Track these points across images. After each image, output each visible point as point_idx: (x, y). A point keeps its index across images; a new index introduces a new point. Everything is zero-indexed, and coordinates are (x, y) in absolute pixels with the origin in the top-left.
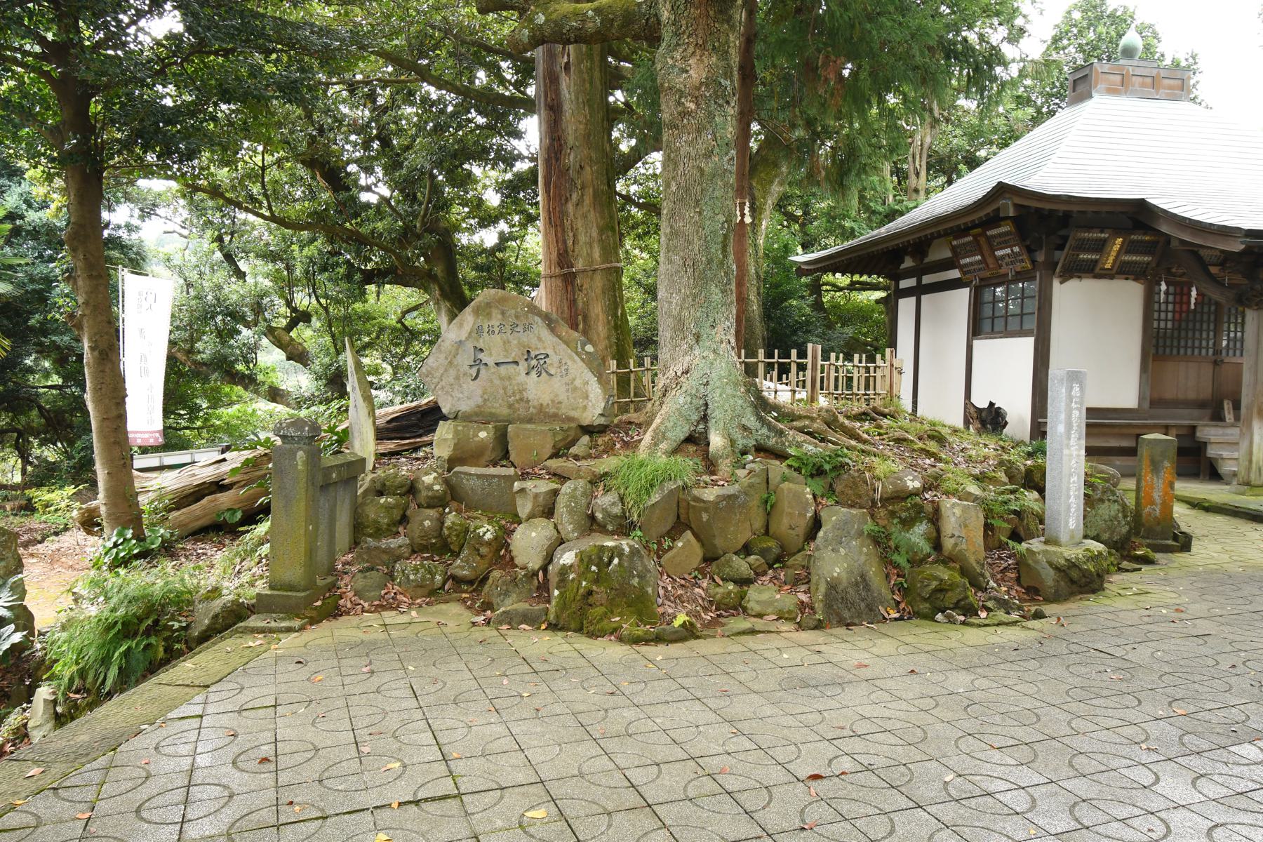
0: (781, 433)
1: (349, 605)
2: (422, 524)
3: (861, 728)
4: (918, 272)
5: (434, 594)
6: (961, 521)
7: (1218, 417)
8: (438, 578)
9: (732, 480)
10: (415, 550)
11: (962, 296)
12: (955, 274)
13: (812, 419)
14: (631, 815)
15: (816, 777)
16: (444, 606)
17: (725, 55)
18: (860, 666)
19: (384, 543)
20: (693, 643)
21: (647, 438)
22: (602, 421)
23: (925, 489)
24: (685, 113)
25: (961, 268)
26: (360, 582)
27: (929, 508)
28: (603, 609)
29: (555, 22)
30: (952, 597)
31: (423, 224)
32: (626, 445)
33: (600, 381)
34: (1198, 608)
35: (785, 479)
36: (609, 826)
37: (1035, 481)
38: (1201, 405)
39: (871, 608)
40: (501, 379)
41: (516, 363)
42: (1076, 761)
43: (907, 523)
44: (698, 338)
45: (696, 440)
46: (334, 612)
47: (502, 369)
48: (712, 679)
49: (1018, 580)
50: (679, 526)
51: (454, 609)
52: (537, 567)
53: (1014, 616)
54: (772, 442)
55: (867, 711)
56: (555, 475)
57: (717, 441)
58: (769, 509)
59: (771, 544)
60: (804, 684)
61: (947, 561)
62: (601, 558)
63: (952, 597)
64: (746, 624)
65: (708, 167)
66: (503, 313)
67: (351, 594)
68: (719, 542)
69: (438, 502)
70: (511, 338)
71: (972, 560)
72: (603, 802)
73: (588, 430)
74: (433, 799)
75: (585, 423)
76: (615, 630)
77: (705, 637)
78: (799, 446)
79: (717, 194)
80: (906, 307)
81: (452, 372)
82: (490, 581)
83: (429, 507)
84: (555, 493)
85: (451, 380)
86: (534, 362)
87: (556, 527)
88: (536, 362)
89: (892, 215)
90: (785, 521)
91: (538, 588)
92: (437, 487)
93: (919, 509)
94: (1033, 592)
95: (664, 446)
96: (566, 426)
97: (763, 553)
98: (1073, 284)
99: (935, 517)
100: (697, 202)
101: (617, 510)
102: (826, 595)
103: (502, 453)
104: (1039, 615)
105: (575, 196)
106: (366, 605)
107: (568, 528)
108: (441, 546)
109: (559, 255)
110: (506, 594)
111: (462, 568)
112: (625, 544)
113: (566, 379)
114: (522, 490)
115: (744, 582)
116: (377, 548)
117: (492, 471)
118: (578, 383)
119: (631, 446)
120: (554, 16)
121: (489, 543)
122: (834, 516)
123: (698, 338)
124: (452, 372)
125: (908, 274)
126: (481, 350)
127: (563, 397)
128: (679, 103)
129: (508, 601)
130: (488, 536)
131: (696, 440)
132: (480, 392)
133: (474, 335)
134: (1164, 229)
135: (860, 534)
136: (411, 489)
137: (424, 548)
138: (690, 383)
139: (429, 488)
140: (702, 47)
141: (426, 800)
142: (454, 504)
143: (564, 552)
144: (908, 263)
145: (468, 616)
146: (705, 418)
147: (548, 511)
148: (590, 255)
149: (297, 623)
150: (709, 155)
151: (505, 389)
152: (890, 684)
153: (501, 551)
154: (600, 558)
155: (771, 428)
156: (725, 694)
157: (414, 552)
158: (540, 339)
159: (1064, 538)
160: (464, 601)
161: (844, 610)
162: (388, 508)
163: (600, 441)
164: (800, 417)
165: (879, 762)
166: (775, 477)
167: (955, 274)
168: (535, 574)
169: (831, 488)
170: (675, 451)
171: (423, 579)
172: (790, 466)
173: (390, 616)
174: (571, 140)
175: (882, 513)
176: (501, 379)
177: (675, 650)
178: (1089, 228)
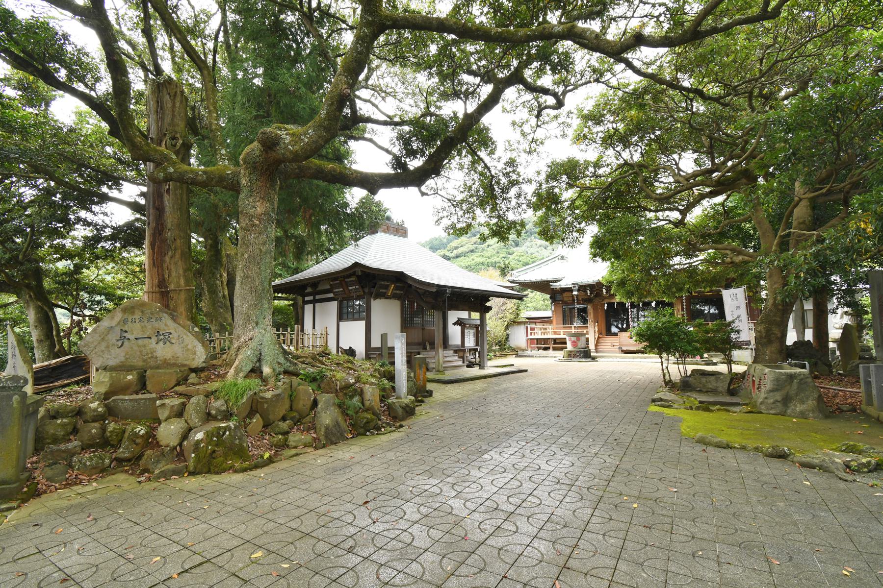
0: (296, 364)
1: (44, 487)
2: (90, 432)
3: (370, 480)
4: (313, 294)
5: (103, 471)
6: (371, 393)
7: (425, 348)
8: (107, 461)
9: (276, 387)
10: (83, 448)
11: (335, 304)
12: (331, 295)
13: (307, 358)
14: (302, 541)
15: (366, 502)
16: (114, 477)
17: (272, 203)
18: (352, 458)
19: (63, 447)
20: (272, 465)
21: (232, 371)
22: (204, 365)
23: (356, 383)
24: (254, 225)
25: (334, 293)
26: (49, 472)
27: (359, 390)
28: (222, 459)
29: (180, 173)
30: (372, 425)
31: (24, 256)
32: (218, 376)
33: (203, 345)
34: (446, 415)
35: (299, 384)
36: (296, 548)
37: (392, 378)
38: (419, 344)
39: (342, 435)
40: (139, 346)
41: (150, 338)
42: (445, 472)
43: (351, 397)
44: (257, 324)
45: (256, 371)
46: (36, 493)
47: (140, 342)
48: (294, 478)
49: (389, 415)
50: (251, 413)
51: (121, 477)
52: (175, 444)
53: (393, 428)
54: (292, 368)
55: (367, 474)
56: (181, 394)
57: (266, 370)
58: (292, 398)
59: (295, 414)
60: (335, 470)
61: (367, 410)
62: (218, 433)
63: (372, 425)
64: (293, 451)
65: (264, 249)
66: (142, 312)
67: (44, 481)
68: (271, 417)
69: (100, 418)
70: (147, 325)
71: (376, 408)
72: (285, 539)
73: (195, 370)
74: (195, 567)
75: (194, 367)
76: (231, 468)
77: (277, 461)
78: (304, 369)
79: (268, 260)
80: (308, 308)
81: (104, 344)
82: (145, 457)
83: (94, 421)
84: (184, 405)
85: (103, 348)
86: (162, 337)
87: (186, 421)
88: (163, 337)
89: (297, 271)
90: (301, 403)
91: (177, 456)
92: (100, 410)
93: (355, 390)
94: (395, 418)
95: (241, 375)
96: (182, 369)
97: (292, 419)
98: (378, 301)
99: (361, 393)
100: (258, 263)
101: (224, 408)
102: (325, 432)
103: (142, 385)
104: (401, 426)
105: (170, 253)
106: (57, 485)
107: (195, 420)
108: (104, 443)
109: (159, 282)
110: (158, 462)
111: (124, 453)
112: (232, 424)
113: (182, 345)
114: (163, 405)
115: (286, 433)
116: (58, 450)
117: (134, 397)
118: (190, 347)
119: (223, 377)
120: (180, 170)
121: (142, 436)
122: (324, 399)
123: (257, 324)
124: (104, 344)
125: (309, 294)
126: (126, 331)
127: (180, 354)
128: (251, 220)
129: (160, 466)
130: (142, 432)
131: (256, 371)
132: (123, 354)
133: (121, 323)
134: (410, 282)
135: (334, 404)
136: (79, 412)
137: (89, 446)
138: (253, 344)
139: (95, 410)
140: (263, 199)
141: (191, 568)
142: (111, 418)
143: (196, 433)
144: (309, 290)
145: (133, 479)
146: (259, 360)
147: (180, 413)
148: (178, 282)
149: (14, 504)
150: (264, 244)
151: (141, 352)
152: (367, 462)
153: (151, 440)
154: (218, 433)
155: (291, 362)
156: (305, 482)
157: (83, 449)
158: (166, 325)
159: (402, 396)
160: (126, 471)
161: (332, 438)
162: (63, 425)
163: (202, 375)
164: (301, 357)
165: (384, 490)
166: (295, 384)
167: (331, 295)
168: (175, 448)
169: (319, 387)
170: (246, 377)
171: (97, 463)
172: (301, 379)
173: (78, 489)
174: (169, 226)
175: (341, 394)
176: (139, 346)
177: (266, 470)
178: (383, 280)
